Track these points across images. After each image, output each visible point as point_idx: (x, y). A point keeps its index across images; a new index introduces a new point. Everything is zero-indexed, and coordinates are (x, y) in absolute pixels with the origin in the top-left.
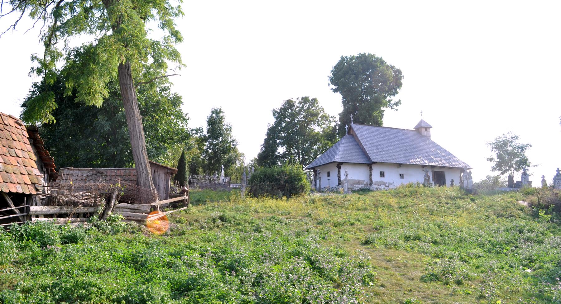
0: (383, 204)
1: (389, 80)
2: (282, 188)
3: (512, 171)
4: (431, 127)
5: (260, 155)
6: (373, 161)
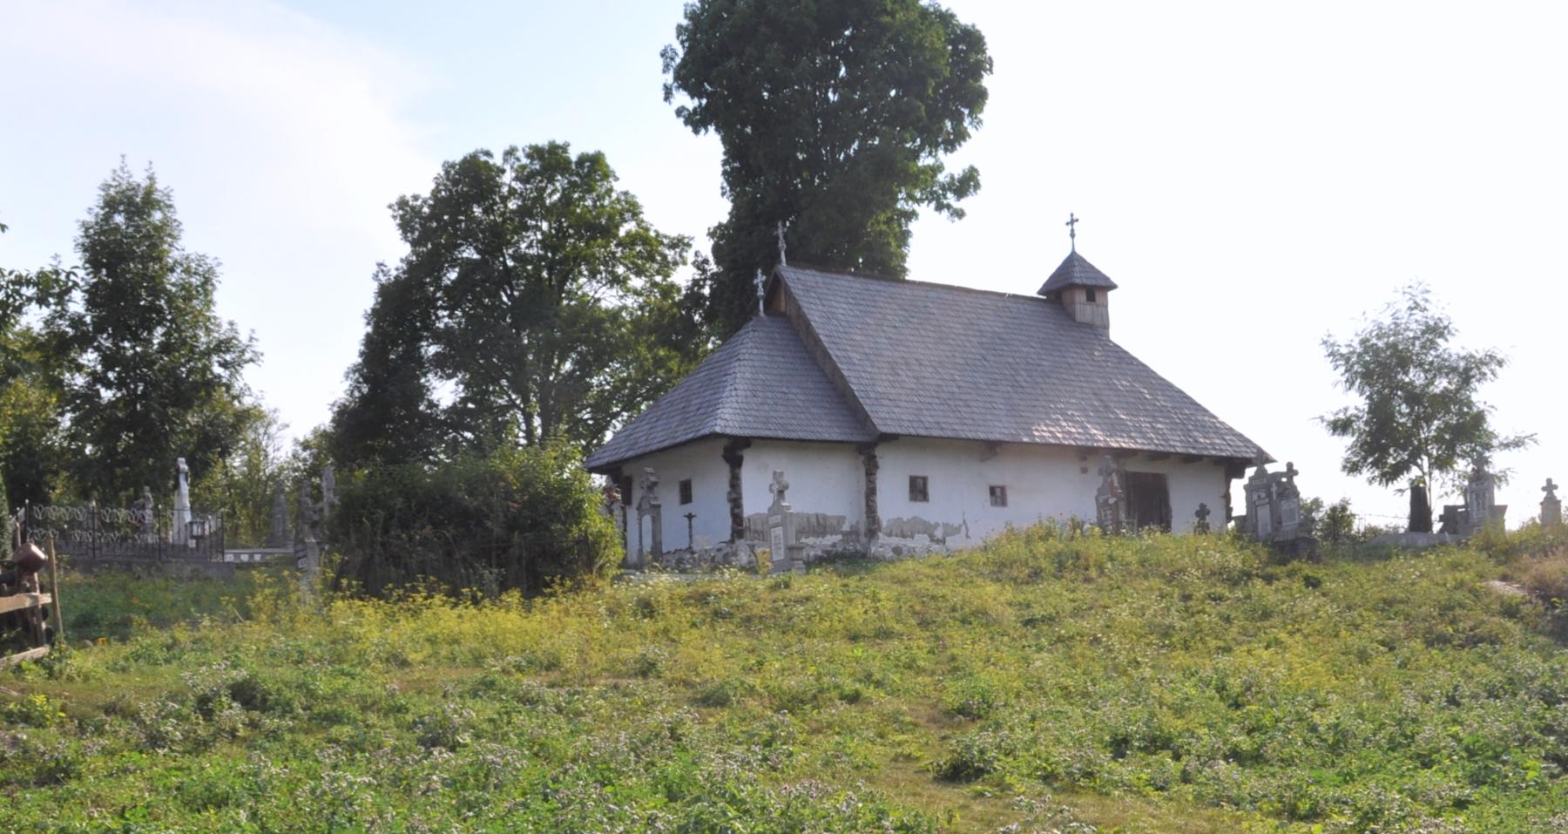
0: (954, 610)
1: (934, 74)
2: (495, 553)
3: (1426, 469)
4: (1113, 287)
5: (343, 416)
6: (883, 429)
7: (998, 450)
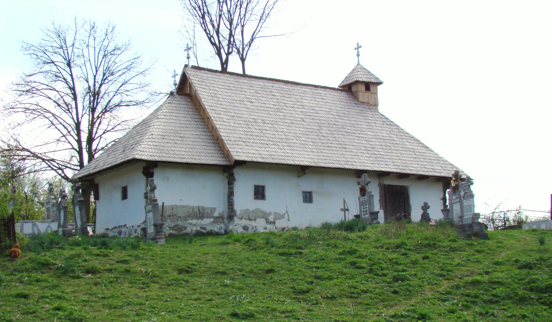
7: (307, 171)
